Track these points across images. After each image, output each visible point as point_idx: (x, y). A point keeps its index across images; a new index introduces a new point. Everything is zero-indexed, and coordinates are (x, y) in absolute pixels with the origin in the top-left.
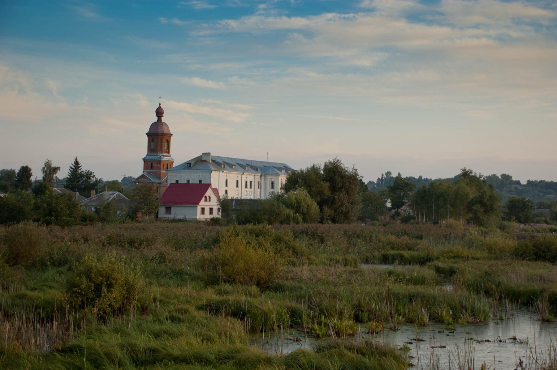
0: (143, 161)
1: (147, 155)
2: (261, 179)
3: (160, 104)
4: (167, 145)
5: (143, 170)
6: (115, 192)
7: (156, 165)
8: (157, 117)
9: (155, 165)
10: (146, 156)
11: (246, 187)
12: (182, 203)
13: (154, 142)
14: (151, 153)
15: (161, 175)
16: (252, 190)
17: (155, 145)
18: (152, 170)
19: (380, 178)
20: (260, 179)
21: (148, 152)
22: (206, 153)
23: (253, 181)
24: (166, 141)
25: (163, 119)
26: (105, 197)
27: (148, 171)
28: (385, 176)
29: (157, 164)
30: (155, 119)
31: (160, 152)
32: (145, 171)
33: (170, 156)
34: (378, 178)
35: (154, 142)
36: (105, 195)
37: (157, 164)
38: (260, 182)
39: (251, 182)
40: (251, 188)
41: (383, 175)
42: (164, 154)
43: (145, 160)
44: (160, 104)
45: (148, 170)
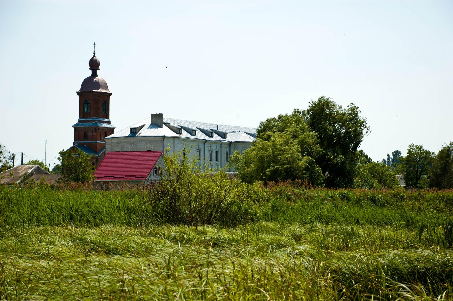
0: (73, 130)
1: (79, 121)
2: (230, 149)
3: (94, 53)
4: (105, 107)
5: (74, 141)
6: (34, 165)
7: (91, 134)
8: (91, 71)
9: (89, 134)
10: (77, 122)
11: (211, 160)
12: (123, 177)
13: (88, 103)
14: (84, 118)
15: (98, 148)
16: (218, 163)
17: (89, 108)
18: (85, 140)
19: (386, 160)
20: (228, 149)
21: (80, 117)
22: (157, 114)
23: (219, 151)
24: (103, 102)
25: (101, 75)
26: (20, 173)
27: (79, 142)
28: (391, 157)
29: (92, 132)
30: (89, 73)
31: (96, 117)
32: (76, 142)
33: (109, 123)
34: (383, 159)
35: (88, 103)
36: (20, 170)
37: (92, 132)
38: (229, 153)
39: (217, 152)
40: (217, 160)
41: (389, 155)
42: (102, 120)
43: (76, 127)
44: (94, 53)
45: (80, 141)
